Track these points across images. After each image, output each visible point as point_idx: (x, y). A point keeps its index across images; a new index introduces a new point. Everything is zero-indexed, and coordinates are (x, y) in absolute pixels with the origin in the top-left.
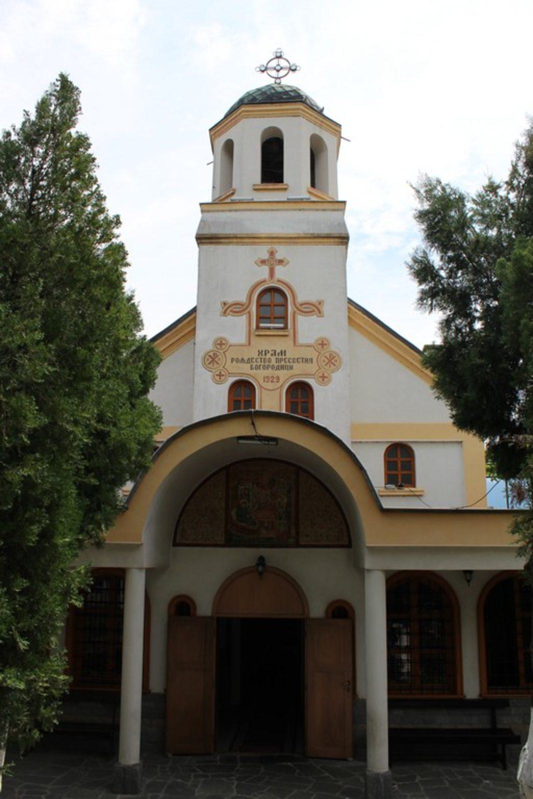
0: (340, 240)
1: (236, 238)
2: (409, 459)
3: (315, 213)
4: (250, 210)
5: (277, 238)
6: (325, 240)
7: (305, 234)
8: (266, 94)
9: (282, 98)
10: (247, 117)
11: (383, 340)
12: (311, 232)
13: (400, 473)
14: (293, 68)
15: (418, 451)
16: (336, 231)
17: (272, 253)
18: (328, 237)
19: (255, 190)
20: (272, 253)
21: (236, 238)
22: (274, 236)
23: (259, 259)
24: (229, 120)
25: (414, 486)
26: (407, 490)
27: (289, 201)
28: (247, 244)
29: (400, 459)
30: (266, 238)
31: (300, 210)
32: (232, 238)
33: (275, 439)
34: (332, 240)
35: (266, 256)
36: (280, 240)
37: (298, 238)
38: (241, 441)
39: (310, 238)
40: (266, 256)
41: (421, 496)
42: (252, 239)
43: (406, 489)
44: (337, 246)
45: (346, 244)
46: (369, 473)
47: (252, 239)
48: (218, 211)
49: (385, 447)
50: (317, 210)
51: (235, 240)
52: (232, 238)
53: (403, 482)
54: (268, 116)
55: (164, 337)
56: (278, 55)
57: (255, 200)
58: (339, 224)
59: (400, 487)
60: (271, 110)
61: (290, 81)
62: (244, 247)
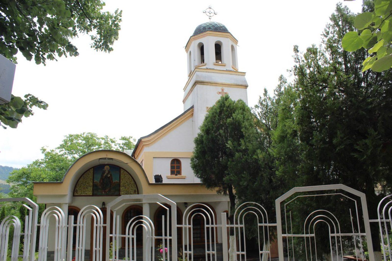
0: (245, 87)
1: (210, 83)
2: (179, 165)
3: (230, 75)
4: (213, 72)
5: (224, 84)
6: (241, 87)
7: (234, 84)
8: (215, 27)
9: (220, 29)
10: (209, 35)
11: (185, 118)
12: (236, 83)
13: (176, 170)
14: (216, 13)
15: (182, 160)
16: (244, 84)
17: (223, 90)
18: (241, 86)
19: (214, 65)
20: (223, 90)
21: (210, 83)
22: (223, 83)
23: (218, 92)
24: (203, 34)
25: (181, 175)
26: (179, 176)
27: (227, 71)
28: (214, 86)
29: (175, 165)
30: (220, 84)
31: (231, 74)
32: (209, 83)
33: (112, 159)
34: (243, 87)
35: (220, 91)
36: (226, 85)
37: (232, 85)
38: (100, 160)
39: (235, 85)
40: (220, 91)
41: (184, 178)
42: (215, 84)
43: (178, 176)
44: (244, 89)
45: (246, 88)
46: (145, 171)
47: (215, 84)
48: (202, 72)
49: (171, 160)
50: (237, 75)
51: (209, 84)
52: (209, 83)
53: (177, 173)
54: (217, 36)
55: (180, 118)
56: (210, 7)
57: (215, 69)
58: (244, 81)
59: (176, 175)
60: (218, 34)
61: (217, 20)
62: (213, 87)
